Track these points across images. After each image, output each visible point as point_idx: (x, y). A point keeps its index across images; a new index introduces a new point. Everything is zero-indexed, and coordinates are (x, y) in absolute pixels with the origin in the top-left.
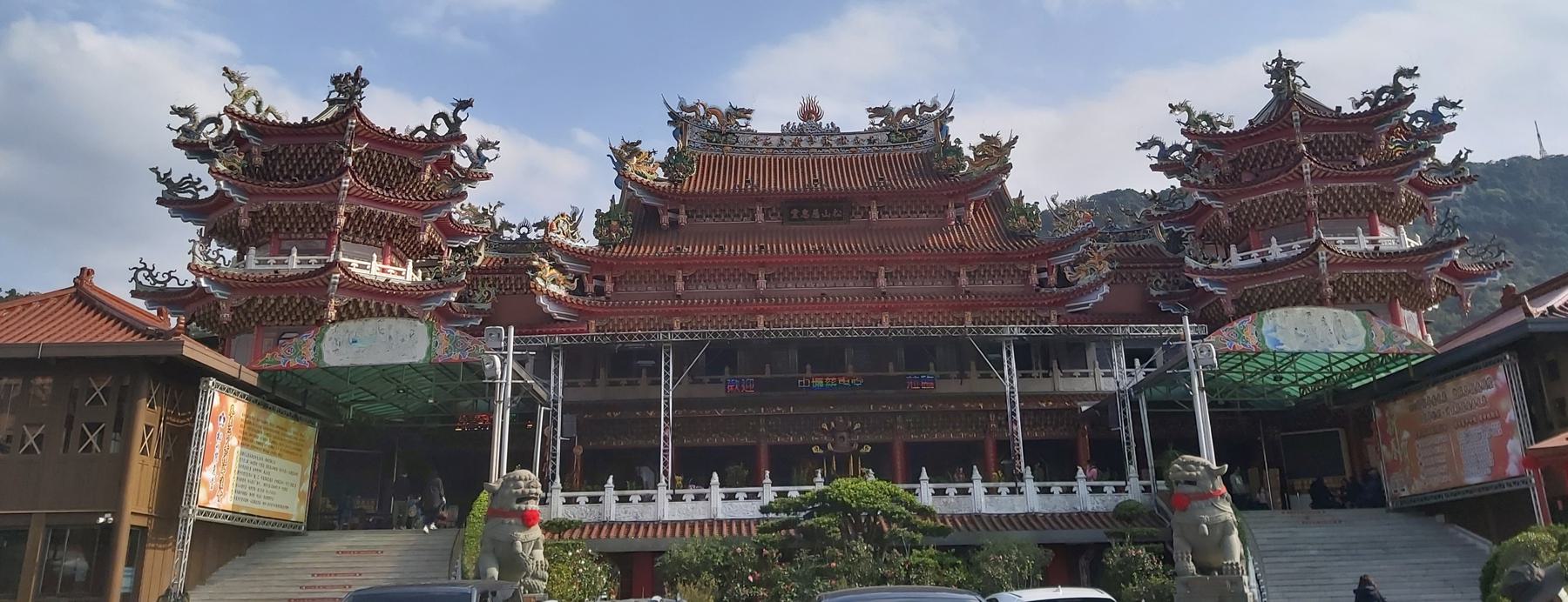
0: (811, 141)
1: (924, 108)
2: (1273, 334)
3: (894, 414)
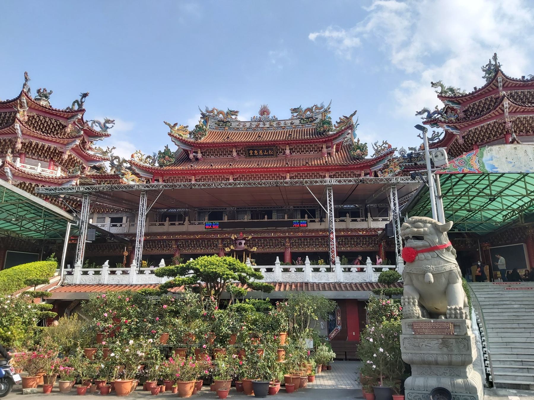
0: (264, 124)
1: (317, 108)
2: (491, 162)
3: (285, 238)
